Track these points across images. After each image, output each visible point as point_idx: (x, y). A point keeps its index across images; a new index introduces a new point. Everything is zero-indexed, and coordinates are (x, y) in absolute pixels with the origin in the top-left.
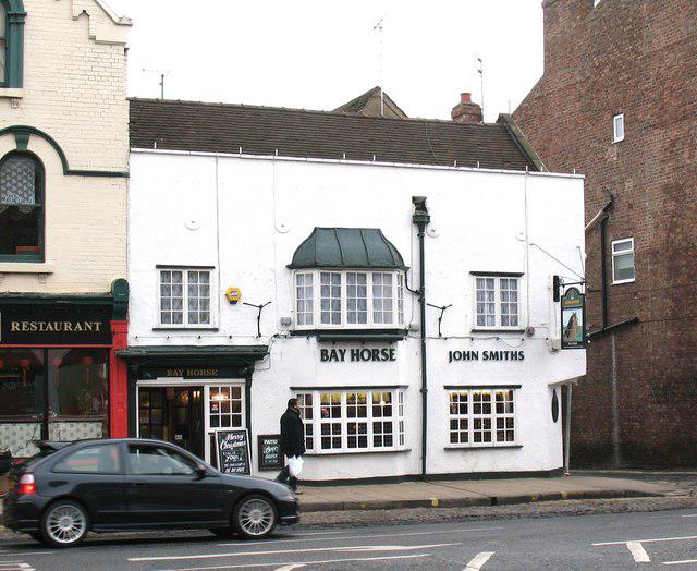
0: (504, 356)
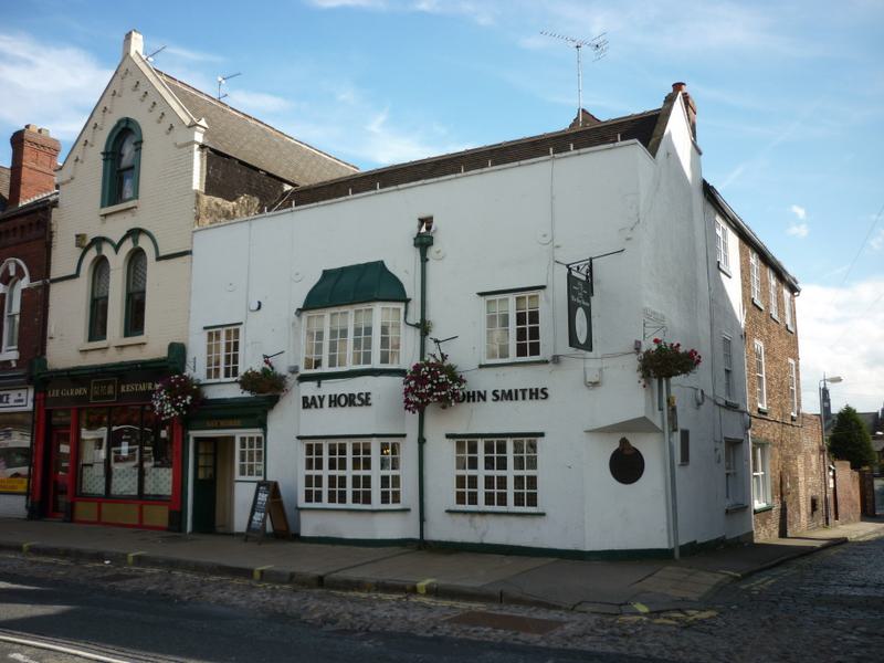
0: (520, 394)
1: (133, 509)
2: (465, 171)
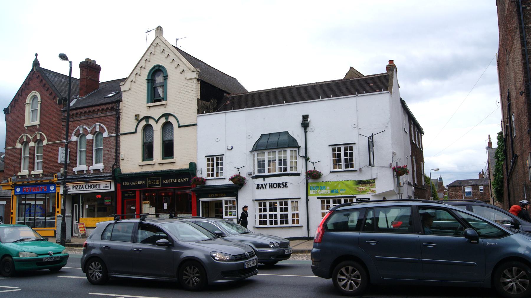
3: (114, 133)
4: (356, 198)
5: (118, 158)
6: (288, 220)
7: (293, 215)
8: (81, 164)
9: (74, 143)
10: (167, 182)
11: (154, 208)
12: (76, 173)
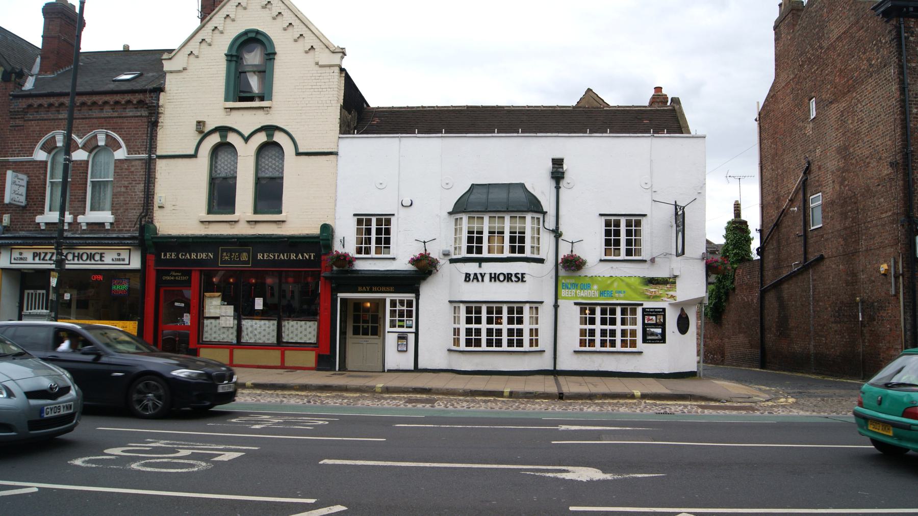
1: (277, 354)
2: (590, 133)
3: (143, 154)
4: (643, 307)
5: (150, 203)
6: (522, 339)
7: (531, 330)
8: (52, 209)
9: (39, 165)
10: (265, 258)
11: (232, 307)
12: (43, 228)
